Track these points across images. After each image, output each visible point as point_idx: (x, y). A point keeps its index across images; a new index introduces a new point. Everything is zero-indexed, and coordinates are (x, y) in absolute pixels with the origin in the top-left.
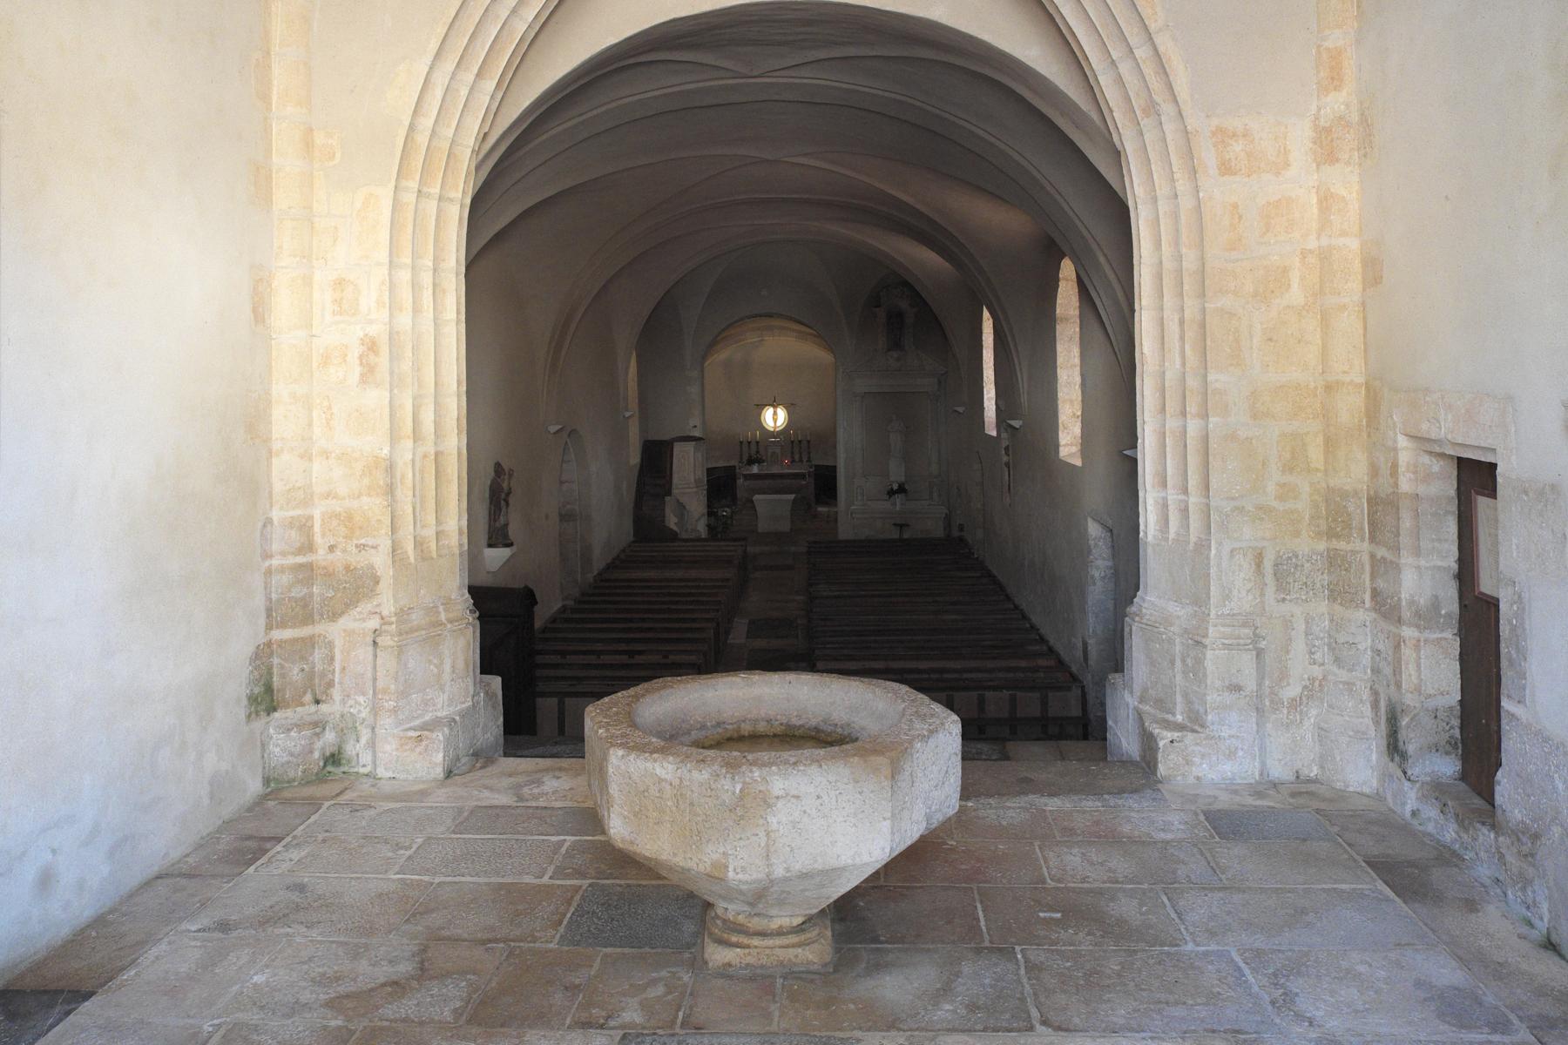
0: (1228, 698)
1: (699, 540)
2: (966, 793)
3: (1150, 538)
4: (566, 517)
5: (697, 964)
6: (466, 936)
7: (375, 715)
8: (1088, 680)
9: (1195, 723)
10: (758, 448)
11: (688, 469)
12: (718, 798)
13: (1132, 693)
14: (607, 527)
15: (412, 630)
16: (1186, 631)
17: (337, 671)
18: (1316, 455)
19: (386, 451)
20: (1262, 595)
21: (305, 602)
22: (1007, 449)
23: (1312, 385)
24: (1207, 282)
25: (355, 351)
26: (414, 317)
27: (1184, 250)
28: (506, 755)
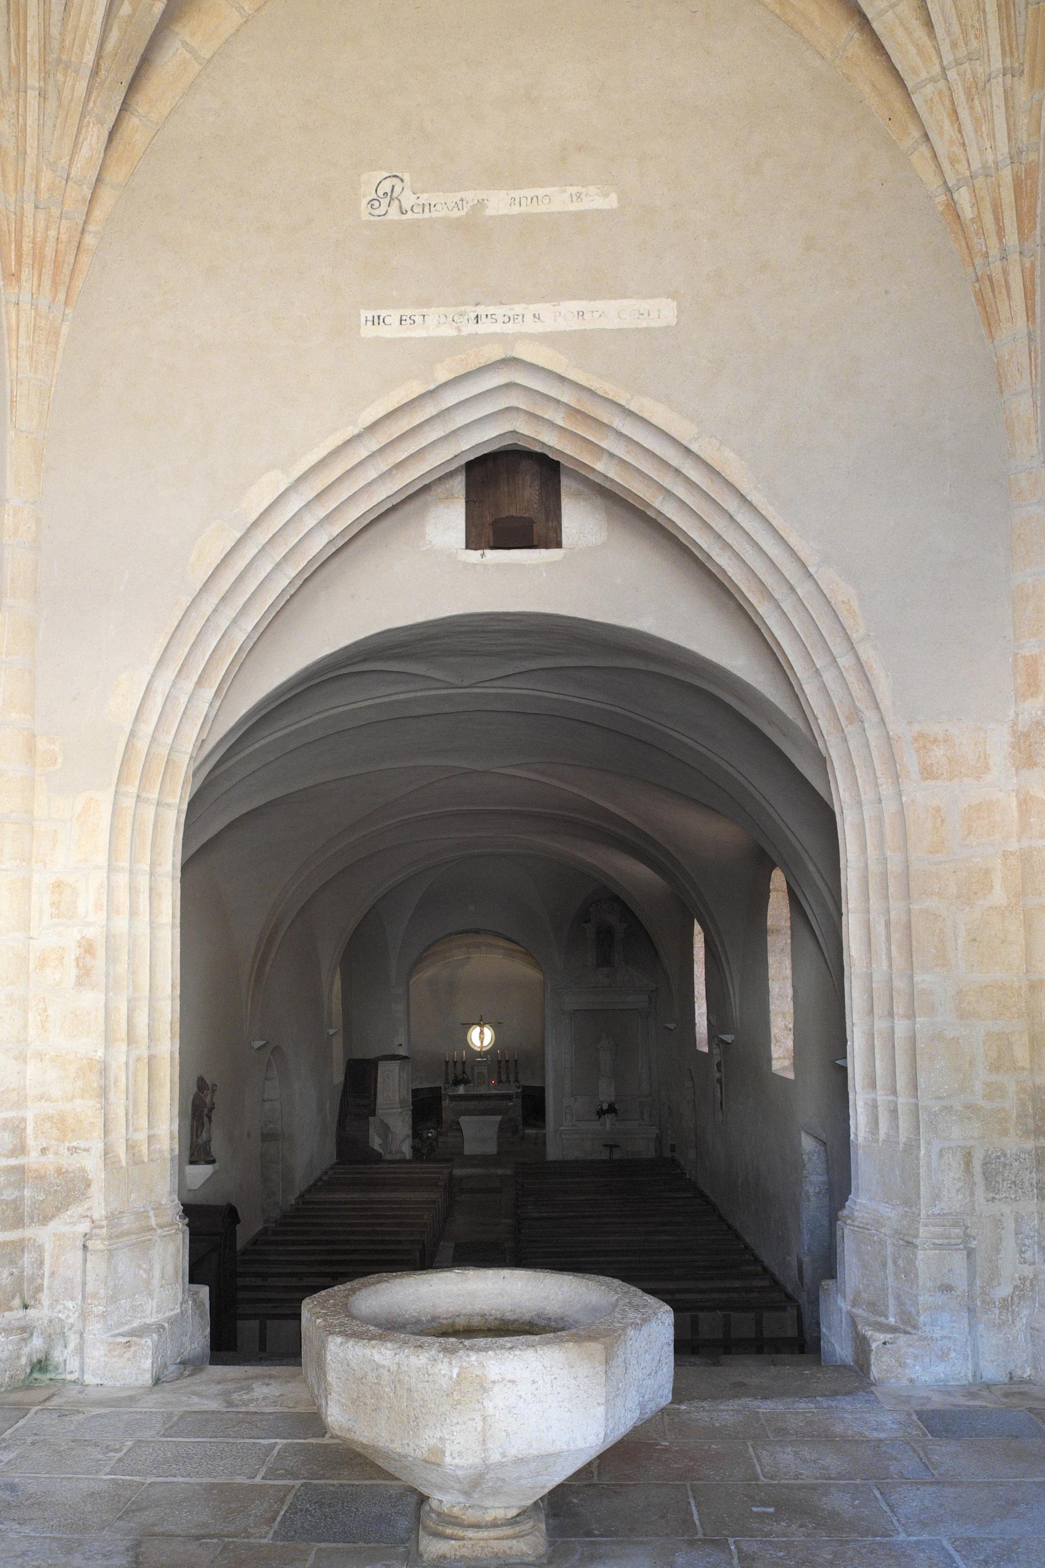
1: (403, 1161)
2: (679, 1394)
3: (860, 1140)
4: (268, 1137)
5: (413, 1556)
6: (179, 1532)
7: (84, 1320)
8: (803, 1299)
9: (908, 1324)
10: (463, 1068)
11: (393, 1089)
12: (435, 1382)
13: (844, 1297)
14: (310, 1152)
15: (123, 1234)
16: (897, 1232)
18: (1021, 1054)
19: (100, 1053)
20: (972, 1194)
21: (16, 1205)
22: (719, 1065)
23: (1016, 985)
24: (912, 884)
26: (130, 920)
27: (889, 853)
28: (211, 1364)
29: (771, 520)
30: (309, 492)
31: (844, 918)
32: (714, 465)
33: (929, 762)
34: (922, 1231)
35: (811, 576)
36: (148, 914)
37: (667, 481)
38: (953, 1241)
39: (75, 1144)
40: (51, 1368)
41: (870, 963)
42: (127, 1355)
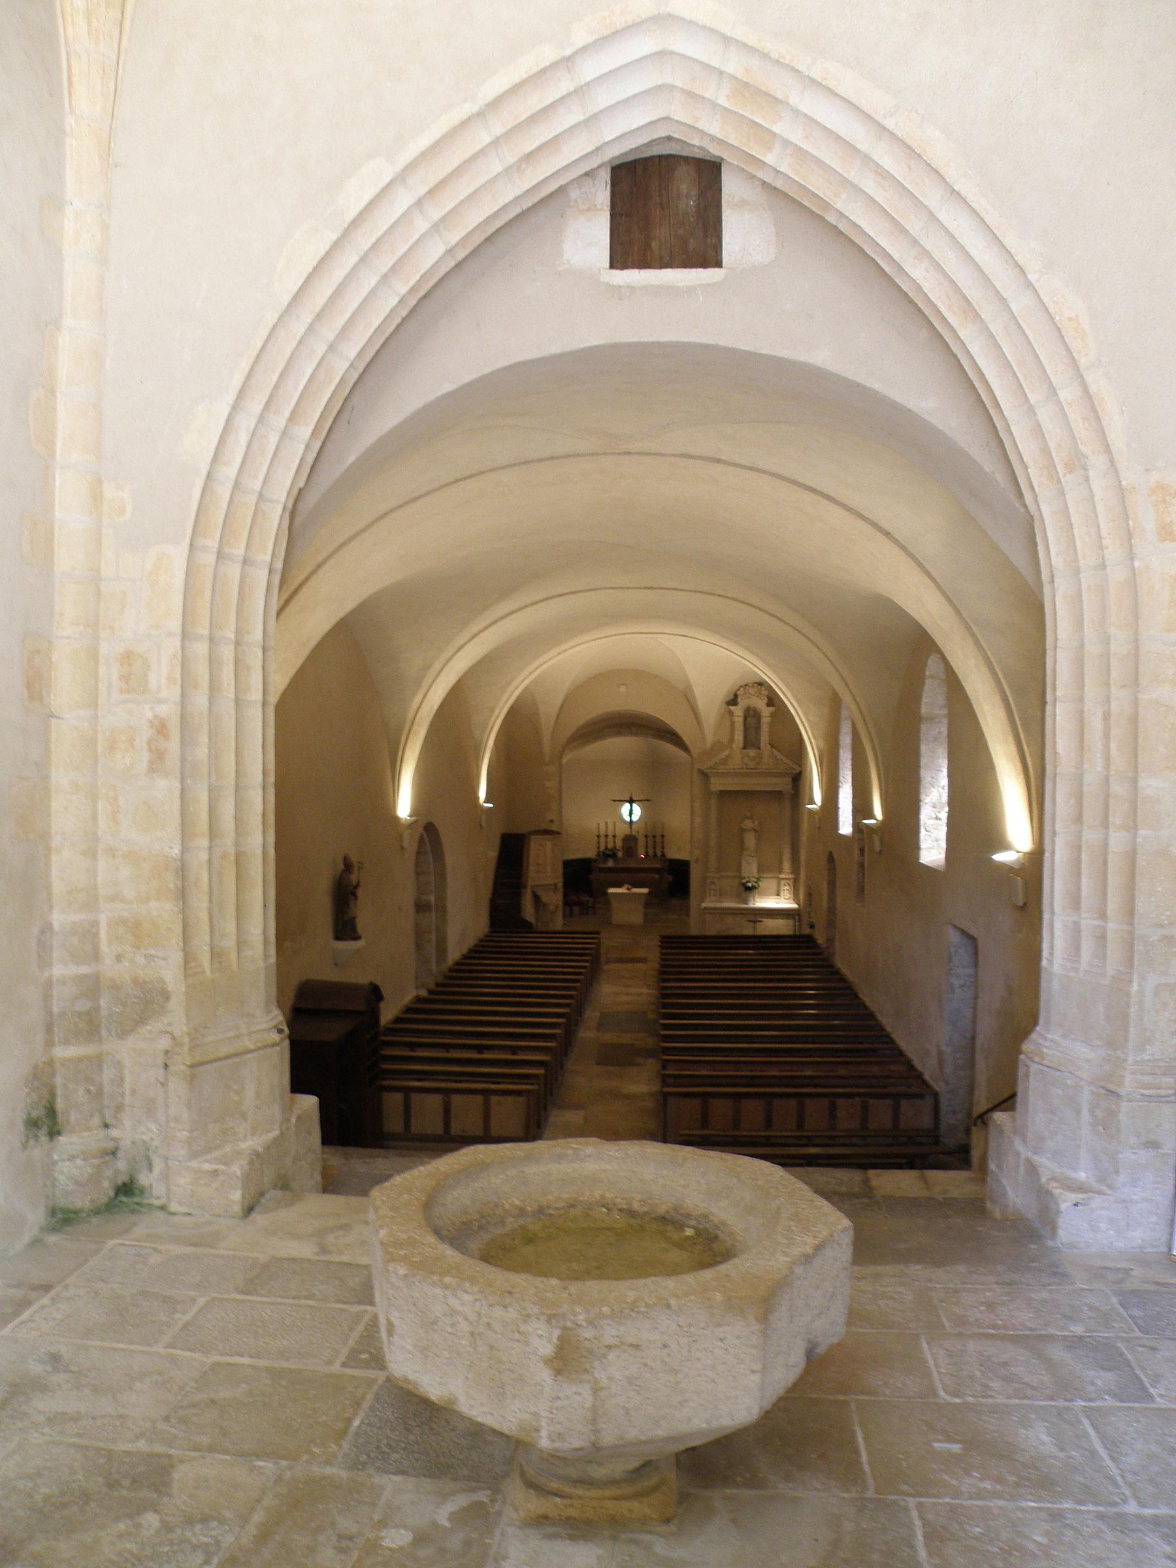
0: (1144, 1156)
3: (1056, 968)
17: (128, 1092)
19: (176, 851)
25: (145, 735)
27: (1112, 631)
29: (983, 214)
30: (419, 185)
31: (1048, 708)
32: (914, 145)
33: (1169, 519)
34: (1128, 1079)
35: (1030, 285)
36: (232, 689)
37: (853, 173)
38: (1163, 1092)
39: (153, 952)
40: (136, 1192)
41: (1081, 762)
42: (215, 1185)
